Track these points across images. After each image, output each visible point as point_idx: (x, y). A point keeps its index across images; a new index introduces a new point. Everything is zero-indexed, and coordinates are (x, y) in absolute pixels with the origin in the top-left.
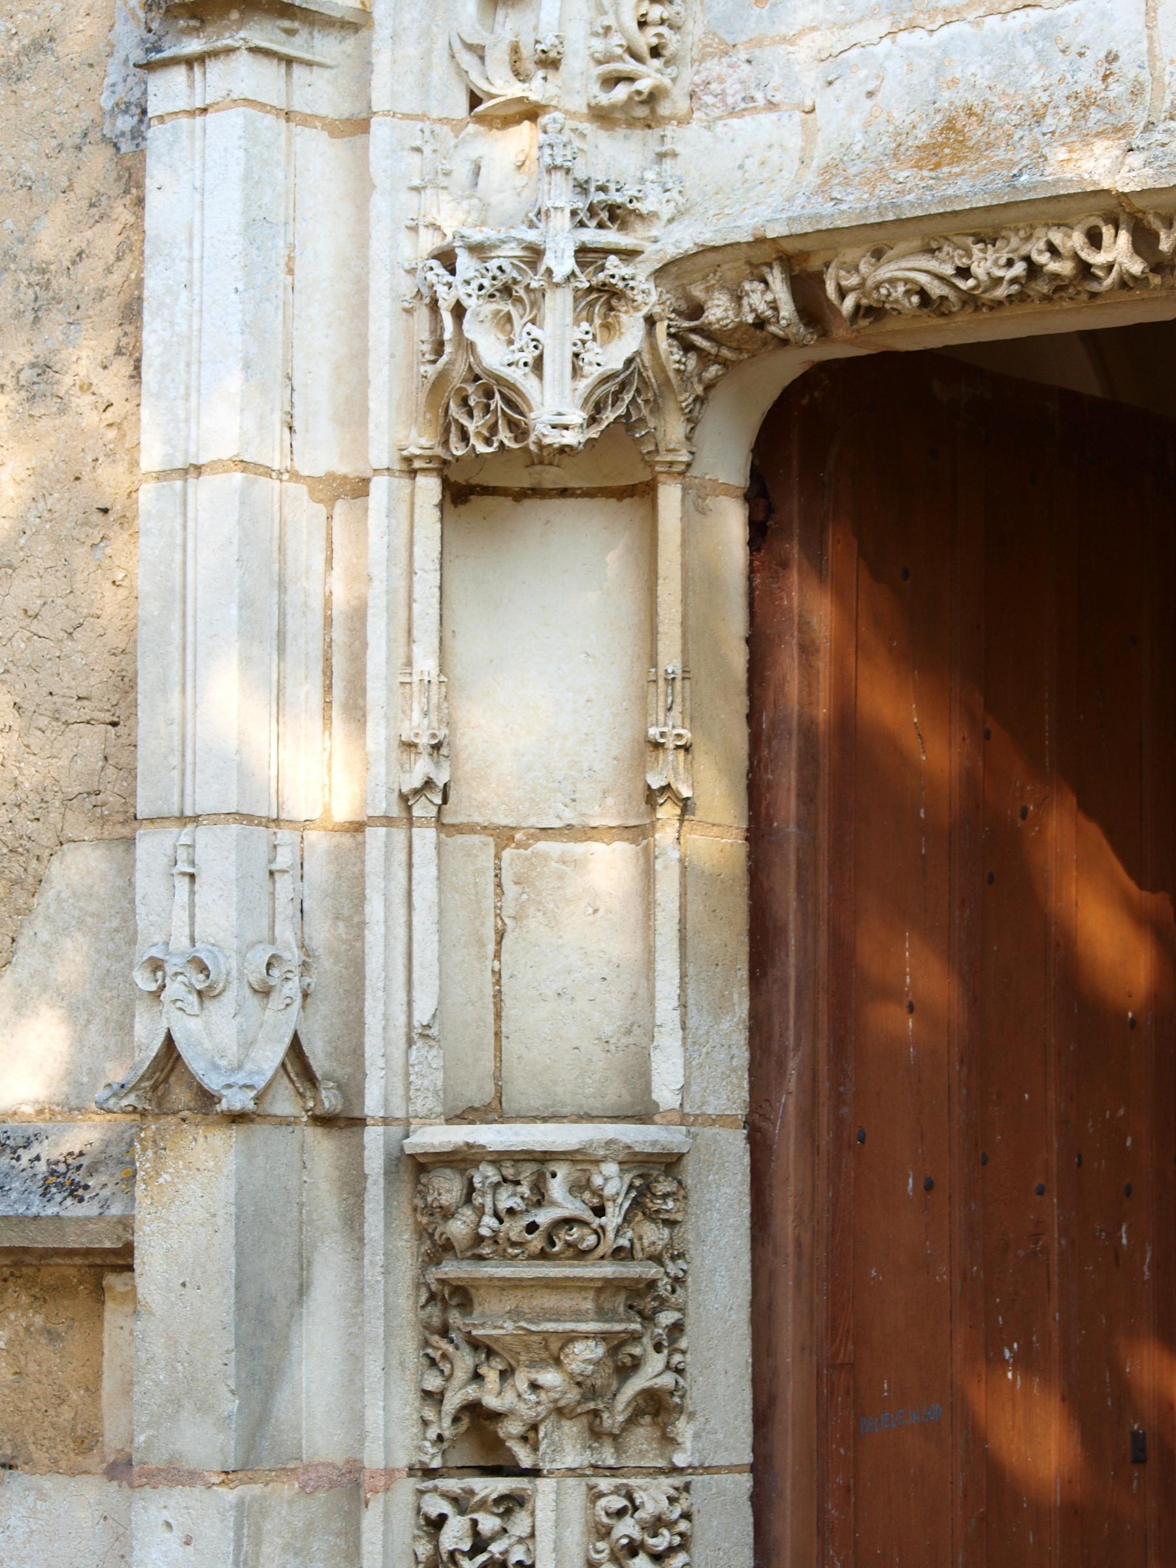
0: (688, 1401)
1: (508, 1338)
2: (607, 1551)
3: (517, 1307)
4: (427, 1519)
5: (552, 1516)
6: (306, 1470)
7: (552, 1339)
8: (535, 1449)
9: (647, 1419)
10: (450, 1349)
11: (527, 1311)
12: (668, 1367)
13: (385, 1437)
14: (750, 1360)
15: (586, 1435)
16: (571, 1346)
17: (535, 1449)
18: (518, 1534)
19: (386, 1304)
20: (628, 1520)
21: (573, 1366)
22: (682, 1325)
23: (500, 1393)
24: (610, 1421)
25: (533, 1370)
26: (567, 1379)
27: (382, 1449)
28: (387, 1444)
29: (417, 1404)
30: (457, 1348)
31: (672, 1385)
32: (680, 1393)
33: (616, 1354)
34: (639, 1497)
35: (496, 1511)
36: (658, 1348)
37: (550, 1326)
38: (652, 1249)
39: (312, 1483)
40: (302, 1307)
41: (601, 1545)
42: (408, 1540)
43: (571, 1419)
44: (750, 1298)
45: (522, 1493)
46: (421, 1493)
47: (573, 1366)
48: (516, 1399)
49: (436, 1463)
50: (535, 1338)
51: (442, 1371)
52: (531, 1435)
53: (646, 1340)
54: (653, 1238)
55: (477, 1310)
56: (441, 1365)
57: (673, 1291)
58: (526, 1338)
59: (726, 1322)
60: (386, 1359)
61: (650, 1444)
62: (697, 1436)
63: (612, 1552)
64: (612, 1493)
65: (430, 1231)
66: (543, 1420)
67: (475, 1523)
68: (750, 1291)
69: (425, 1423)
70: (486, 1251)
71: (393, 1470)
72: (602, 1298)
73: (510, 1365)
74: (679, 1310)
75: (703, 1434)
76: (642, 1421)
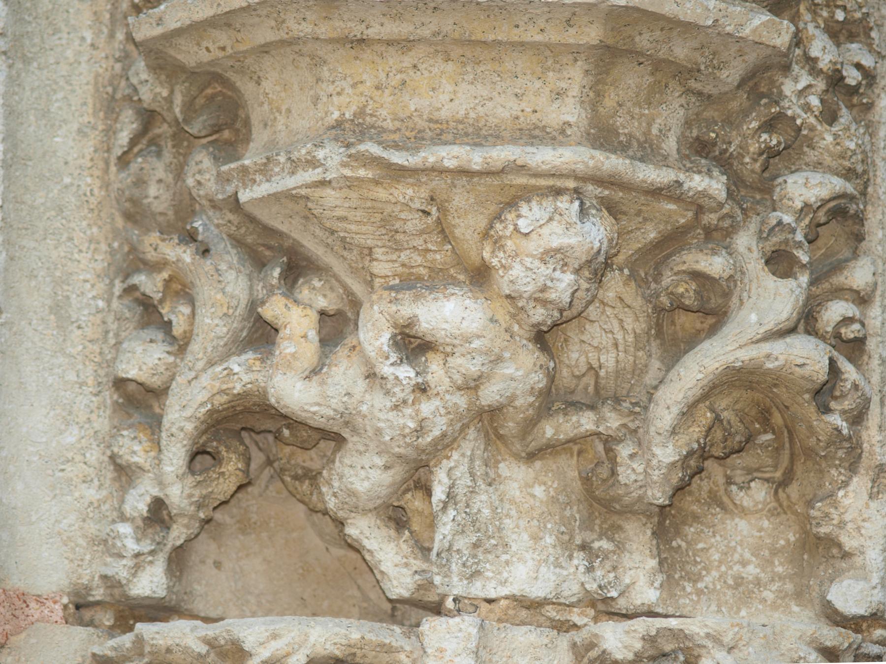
1: (331, 196)
7: (459, 199)
9: (759, 493)
10: (186, 255)
11: (389, 124)
15: (575, 512)
21: (517, 271)
23: (315, 371)
25: (407, 295)
26: (503, 317)
29: (102, 423)
31: (818, 369)
32: (847, 404)
43: (531, 457)
48: (362, 384)
50: (405, 192)
51: (167, 326)
52: (414, 501)
55: (260, 137)
56: (165, 310)
58: (381, 193)
71: (23, 597)
73: (349, 292)
74: (849, 174)
76: (743, 498)
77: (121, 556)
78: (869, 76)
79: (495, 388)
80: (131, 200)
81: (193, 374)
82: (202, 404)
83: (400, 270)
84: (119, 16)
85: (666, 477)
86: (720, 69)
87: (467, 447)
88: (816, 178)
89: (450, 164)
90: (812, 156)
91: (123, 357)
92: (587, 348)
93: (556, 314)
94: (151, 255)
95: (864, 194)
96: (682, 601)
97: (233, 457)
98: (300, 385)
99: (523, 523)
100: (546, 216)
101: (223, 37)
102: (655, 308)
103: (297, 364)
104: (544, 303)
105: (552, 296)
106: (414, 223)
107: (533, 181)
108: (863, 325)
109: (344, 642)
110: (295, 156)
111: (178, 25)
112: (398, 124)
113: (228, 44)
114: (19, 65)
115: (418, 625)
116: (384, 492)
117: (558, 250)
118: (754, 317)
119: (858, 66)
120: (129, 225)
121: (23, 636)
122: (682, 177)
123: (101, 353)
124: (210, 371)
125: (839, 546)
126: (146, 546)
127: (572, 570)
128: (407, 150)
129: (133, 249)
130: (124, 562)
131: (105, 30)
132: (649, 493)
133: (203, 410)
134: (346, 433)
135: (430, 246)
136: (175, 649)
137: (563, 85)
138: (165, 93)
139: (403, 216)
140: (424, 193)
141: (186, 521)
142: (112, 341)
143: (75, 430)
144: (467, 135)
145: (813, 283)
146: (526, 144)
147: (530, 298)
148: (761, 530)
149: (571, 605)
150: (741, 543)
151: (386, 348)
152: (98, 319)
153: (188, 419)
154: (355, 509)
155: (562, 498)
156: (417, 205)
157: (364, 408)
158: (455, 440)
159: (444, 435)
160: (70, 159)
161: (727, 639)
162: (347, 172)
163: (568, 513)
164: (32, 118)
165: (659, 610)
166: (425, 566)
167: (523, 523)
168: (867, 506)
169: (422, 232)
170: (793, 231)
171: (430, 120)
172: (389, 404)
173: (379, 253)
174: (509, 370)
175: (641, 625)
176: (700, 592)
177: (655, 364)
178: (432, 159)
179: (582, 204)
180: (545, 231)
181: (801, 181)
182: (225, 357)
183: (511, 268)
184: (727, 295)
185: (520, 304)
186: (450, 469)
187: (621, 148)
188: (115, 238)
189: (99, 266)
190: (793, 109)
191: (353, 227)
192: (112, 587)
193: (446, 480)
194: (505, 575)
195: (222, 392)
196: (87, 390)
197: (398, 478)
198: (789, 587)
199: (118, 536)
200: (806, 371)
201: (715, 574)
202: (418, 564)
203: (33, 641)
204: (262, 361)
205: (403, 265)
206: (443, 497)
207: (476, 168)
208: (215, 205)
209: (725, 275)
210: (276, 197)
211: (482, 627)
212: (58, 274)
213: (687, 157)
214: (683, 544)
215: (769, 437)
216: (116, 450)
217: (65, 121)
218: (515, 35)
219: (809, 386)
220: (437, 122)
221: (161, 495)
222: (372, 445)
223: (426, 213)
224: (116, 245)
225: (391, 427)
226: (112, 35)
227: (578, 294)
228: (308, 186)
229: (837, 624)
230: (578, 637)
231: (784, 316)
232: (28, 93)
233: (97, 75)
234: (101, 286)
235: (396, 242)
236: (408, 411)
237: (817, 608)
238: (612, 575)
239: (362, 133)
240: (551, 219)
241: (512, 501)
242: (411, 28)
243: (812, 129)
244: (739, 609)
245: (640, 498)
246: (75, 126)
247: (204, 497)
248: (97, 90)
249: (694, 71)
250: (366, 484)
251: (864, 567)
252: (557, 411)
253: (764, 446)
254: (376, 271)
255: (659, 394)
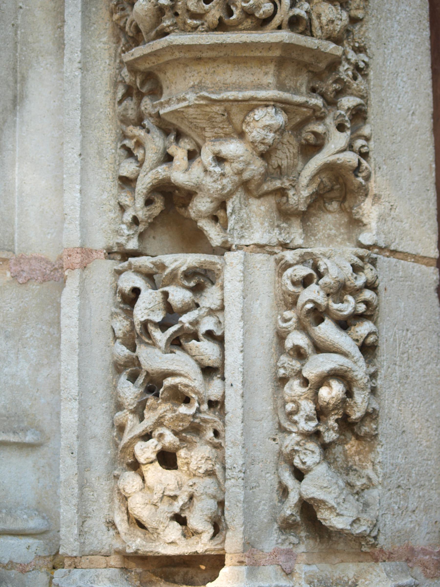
0: (372, 185)
1: (191, 111)
2: (294, 320)
3: (200, 82)
4: (123, 296)
5: (240, 286)
6: (18, 261)
8: (225, 227)
9: (335, 205)
10: (142, 133)
11: (210, 86)
12: (350, 147)
13: (81, 218)
14: (434, 166)
15: (275, 215)
16: (251, 114)
17: (225, 227)
18: (208, 305)
19: (83, 97)
20: (313, 287)
21: (255, 133)
22: (365, 112)
23: (187, 170)
24: (296, 198)
25: (217, 143)
27: (78, 229)
28: (84, 225)
29: (115, 191)
30: (148, 132)
31: (355, 163)
32: (364, 174)
33: (300, 134)
34: (322, 265)
35: (186, 284)
36: (341, 128)
37: (231, 95)
38: (331, 27)
39: (25, 275)
40: (15, 115)
41: (288, 314)
42: (106, 317)
43: (259, 197)
44: (431, 110)
45: (212, 267)
46: (119, 273)
47: (255, 133)
48: (203, 174)
49: (133, 245)
50: (217, 108)
52: (221, 214)
53: (329, 121)
54: (331, 16)
55: (166, 92)
57: (355, 78)
58: (208, 109)
59: (409, 124)
60: (83, 147)
61: (338, 229)
62: (382, 218)
63: (299, 320)
64: (298, 263)
65: (122, 24)
66: (231, 194)
67: (166, 295)
68: (432, 105)
69: (123, 208)
70: (167, 23)
71: (91, 251)
72: (283, 75)
74: (362, 97)
75: (389, 219)
77: (123, 236)
78: (367, 64)
79: (248, 173)
80: (123, 116)
81: (145, 173)
82: (149, 183)
83: (215, 135)
84: (118, 54)
85: (305, 201)
86: (319, 63)
87: (238, 194)
88: (352, 98)
89: (231, 98)
90: (350, 91)
91: (122, 169)
92: (278, 159)
93: (268, 147)
94: (130, 134)
95: (367, 104)
96: (310, 243)
97: (159, 201)
98: (182, 175)
99: (257, 219)
100: (264, 114)
101: (153, 59)
102: (300, 144)
103: (181, 168)
104: (263, 143)
105: (266, 141)
106: (219, 119)
107: (259, 103)
108: (368, 147)
109: (199, 261)
110: (179, 97)
111: (139, 56)
112: (213, 85)
113: (155, 61)
114: (85, 72)
115: (223, 255)
116: (210, 210)
117: (268, 126)
118: (333, 146)
119: (363, 61)
120: (122, 124)
121: (91, 264)
122: (308, 100)
123: (114, 168)
124: (151, 172)
125: (362, 222)
126: (131, 232)
127: (274, 234)
128: (217, 94)
129: (123, 132)
130: (124, 238)
131: (113, 59)
132: (300, 207)
133: (149, 185)
134: (197, 191)
135: (225, 126)
136: (142, 266)
137: (267, 70)
138: (134, 79)
139: (215, 116)
140: (222, 108)
141: (144, 223)
142: (118, 164)
143: (106, 193)
144: (236, 88)
145: (352, 134)
146: (256, 90)
147: (259, 142)
148: (336, 218)
149: (274, 246)
150: (329, 223)
151: (211, 161)
152: (113, 156)
153: (144, 188)
154: (201, 217)
155: (270, 210)
156: (220, 112)
157: (204, 182)
158: (234, 192)
159: (231, 190)
160: (102, 103)
161: (328, 255)
162: (197, 102)
163: (272, 215)
164: (90, 90)
165: (303, 246)
166: (225, 235)
167: (257, 219)
168: (371, 208)
169: (222, 122)
170: (344, 117)
171: (224, 84)
172: (212, 180)
173: (207, 129)
174: (252, 167)
175: (298, 251)
176: (316, 240)
177: (300, 163)
178: (225, 97)
179: (276, 110)
180: (264, 119)
181: (347, 100)
182: (156, 166)
183: (252, 132)
184: (324, 139)
185: (256, 144)
186: (233, 202)
187: (288, 91)
188: (117, 129)
189: (112, 138)
190: (343, 76)
191: (199, 121)
192: (120, 246)
193: (232, 206)
194: (252, 237)
195: (155, 179)
196: (110, 180)
197: (215, 205)
198: (346, 237)
199: (122, 229)
200: (351, 163)
201: (321, 233)
202: (222, 234)
203: (95, 265)
204: (169, 167)
205: (216, 133)
206: (231, 211)
207: (240, 99)
208: (150, 115)
209: (323, 132)
210: (172, 112)
211: (245, 255)
212: (99, 141)
213: (309, 93)
214: (311, 224)
215: (338, 186)
216: (120, 200)
217: (100, 90)
218: (252, 54)
219: (352, 168)
220: (226, 84)
221: (135, 214)
222: (207, 195)
223: (223, 115)
224: (118, 131)
225: (213, 188)
226: (115, 61)
227: (276, 140)
228: (183, 108)
229: (362, 248)
230: (277, 257)
231: (343, 145)
232: (88, 81)
233: (111, 74)
234: (113, 145)
235: (213, 125)
236: (219, 182)
237: (355, 243)
238: (287, 235)
239: (201, 89)
240: (265, 115)
241: (254, 212)
242: (217, 53)
243: (349, 82)
244: (329, 245)
245: (297, 209)
246: (104, 92)
247: (150, 215)
248: (111, 79)
249: (311, 64)
250: (205, 208)
251: (370, 229)
252: (268, 180)
253: (337, 189)
254: (206, 135)
255: (302, 173)
